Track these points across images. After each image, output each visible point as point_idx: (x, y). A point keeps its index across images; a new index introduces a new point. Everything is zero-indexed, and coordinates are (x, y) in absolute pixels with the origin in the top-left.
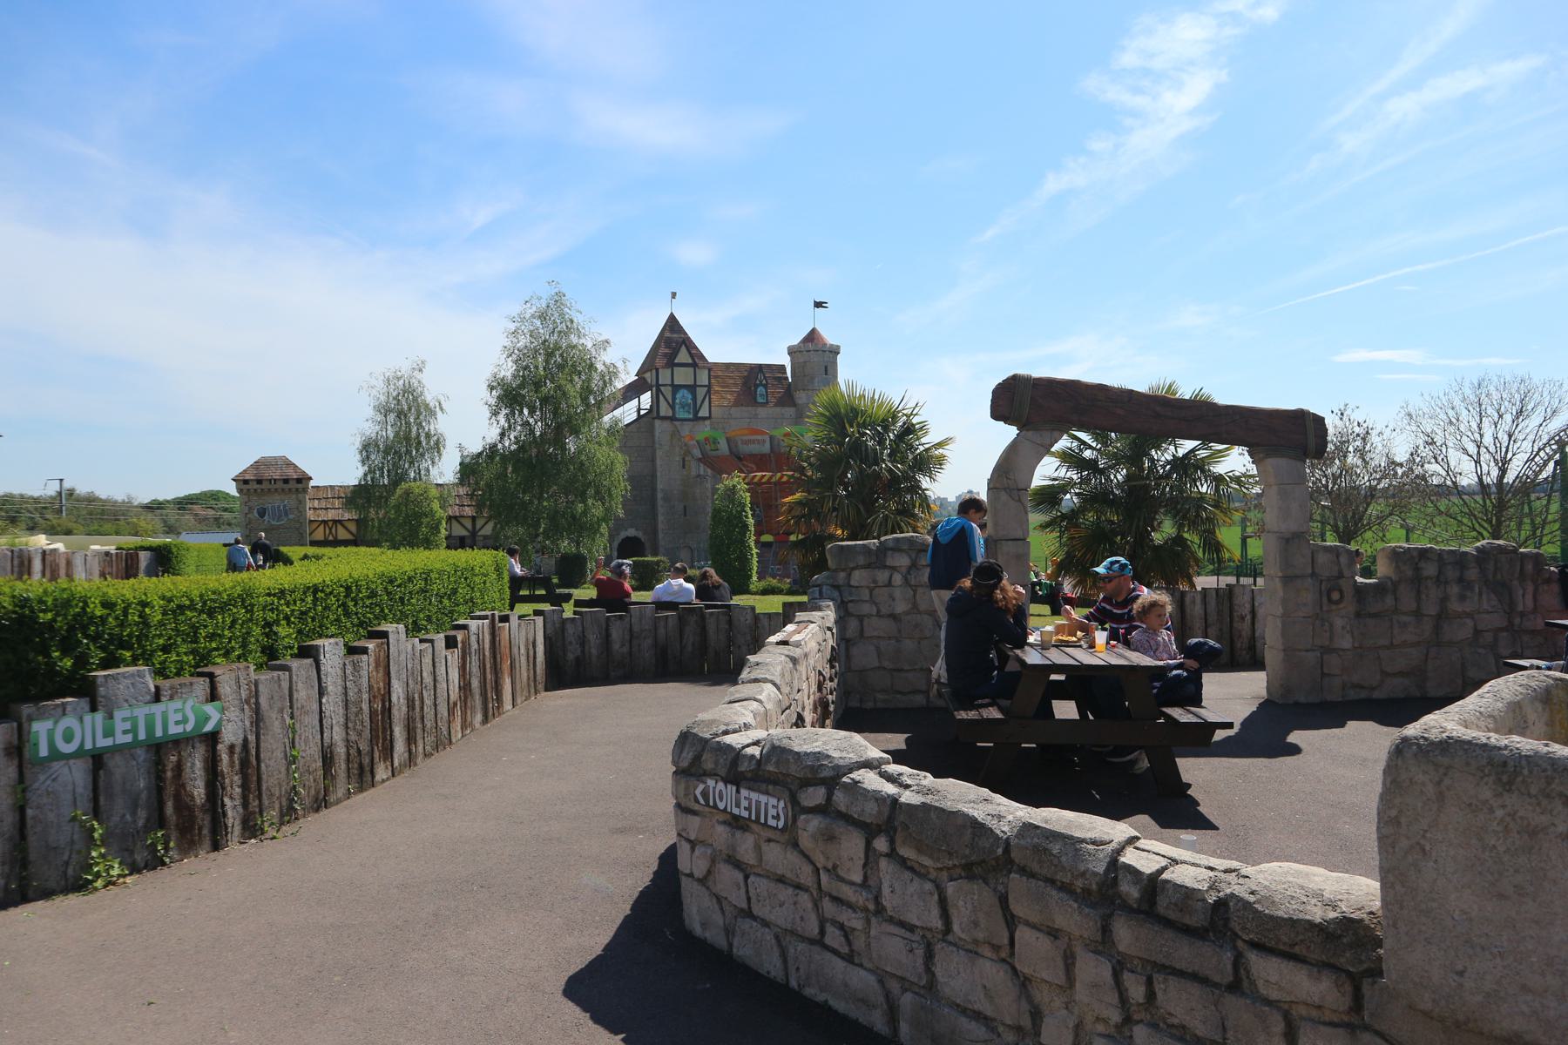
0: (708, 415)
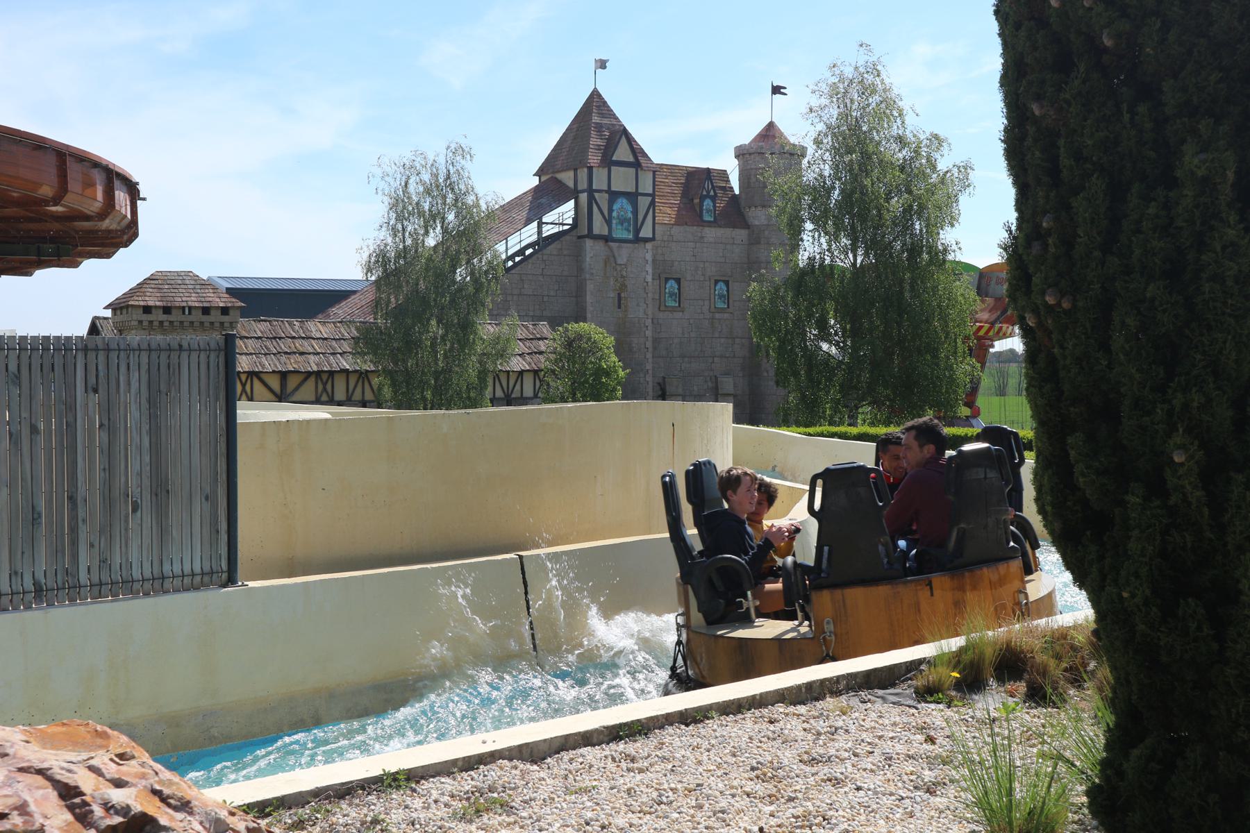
0: (651, 236)
